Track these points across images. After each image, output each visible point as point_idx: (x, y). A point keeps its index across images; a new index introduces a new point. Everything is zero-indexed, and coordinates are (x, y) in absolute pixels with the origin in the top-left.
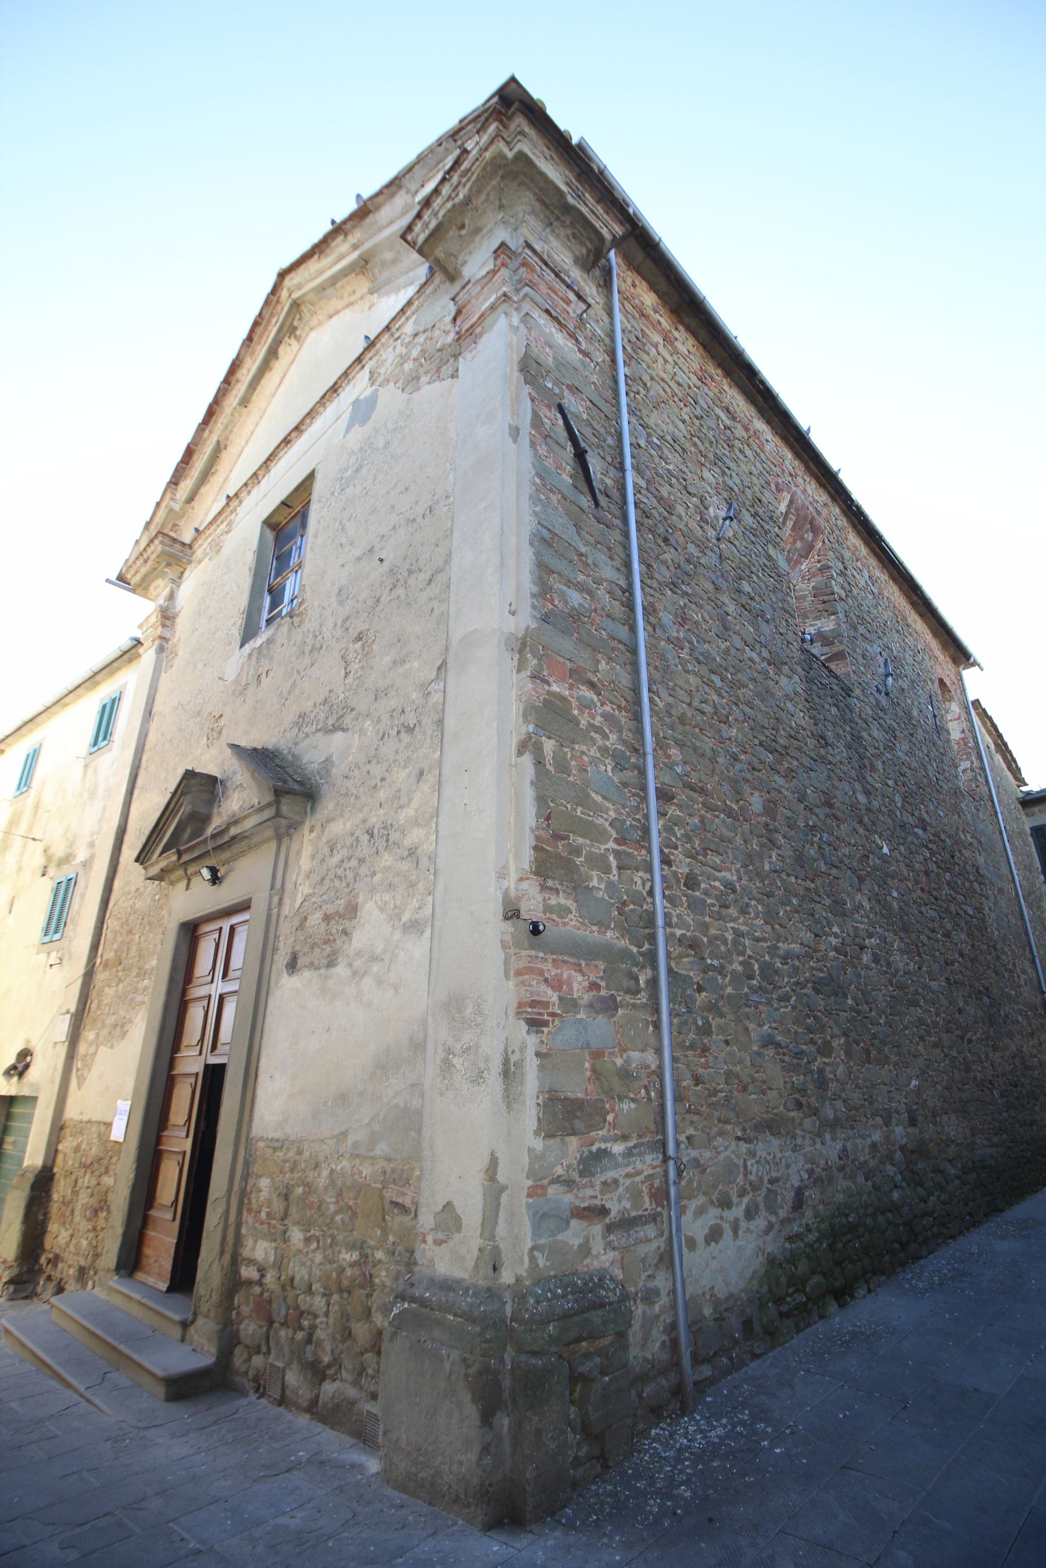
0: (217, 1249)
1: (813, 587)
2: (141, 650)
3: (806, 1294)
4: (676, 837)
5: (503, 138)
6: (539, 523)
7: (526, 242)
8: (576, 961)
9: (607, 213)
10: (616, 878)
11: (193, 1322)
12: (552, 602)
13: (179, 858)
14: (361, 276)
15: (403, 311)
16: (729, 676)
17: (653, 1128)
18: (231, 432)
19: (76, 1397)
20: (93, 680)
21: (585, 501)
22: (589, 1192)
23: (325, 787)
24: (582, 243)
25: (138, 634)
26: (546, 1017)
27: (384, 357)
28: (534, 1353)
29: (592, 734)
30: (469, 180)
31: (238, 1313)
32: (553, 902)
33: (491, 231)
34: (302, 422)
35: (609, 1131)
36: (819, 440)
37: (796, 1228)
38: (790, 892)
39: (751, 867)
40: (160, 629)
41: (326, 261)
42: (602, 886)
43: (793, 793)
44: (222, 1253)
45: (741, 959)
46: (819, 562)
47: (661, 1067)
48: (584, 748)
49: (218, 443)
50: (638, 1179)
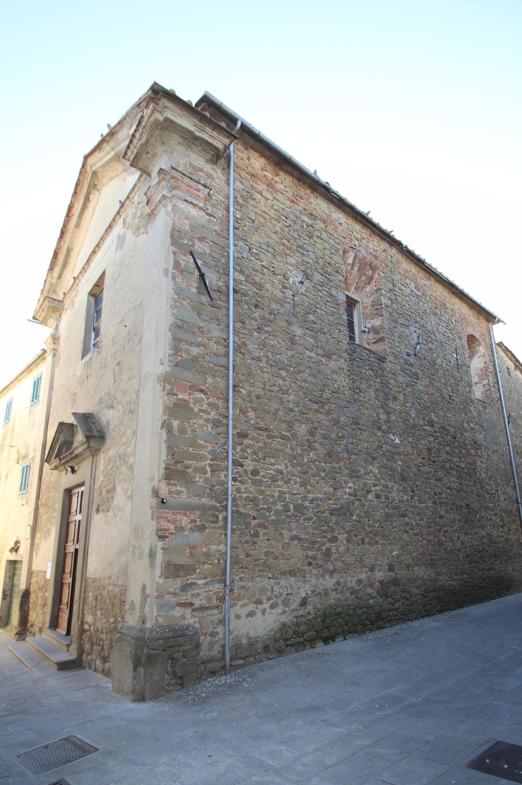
0: (76, 619)
1: (372, 301)
2: (46, 355)
3: (303, 638)
4: (248, 454)
5: (157, 111)
6: (176, 318)
7: (171, 167)
8: (185, 512)
9: (219, 134)
10: (210, 475)
11: (70, 645)
12: (181, 356)
13: (60, 462)
14: (118, 163)
15: (133, 189)
16: (292, 369)
17: (221, 574)
18: (74, 241)
19: (28, 670)
20: (29, 368)
21: (205, 299)
22: (186, 597)
23: (107, 434)
24: (208, 153)
25: (44, 347)
26: (167, 535)
27: (128, 212)
28: (153, 650)
29: (201, 414)
30: (146, 131)
31: (84, 641)
32: (174, 489)
33: (160, 155)
34: (99, 243)
35: (197, 576)
36: (375, 218)
37: (301, 613)
38: (320, 469)
39: (295, 461)
40: (53, 345)
41: (103, 153)
42: (202, 480)
43: (330, 421)
44: (78, 620)
45: (282, 504)
46: (376, 286)
47: (226, 551)
48: (196, 421)
49: (68, 248)
50: (210, 593)
